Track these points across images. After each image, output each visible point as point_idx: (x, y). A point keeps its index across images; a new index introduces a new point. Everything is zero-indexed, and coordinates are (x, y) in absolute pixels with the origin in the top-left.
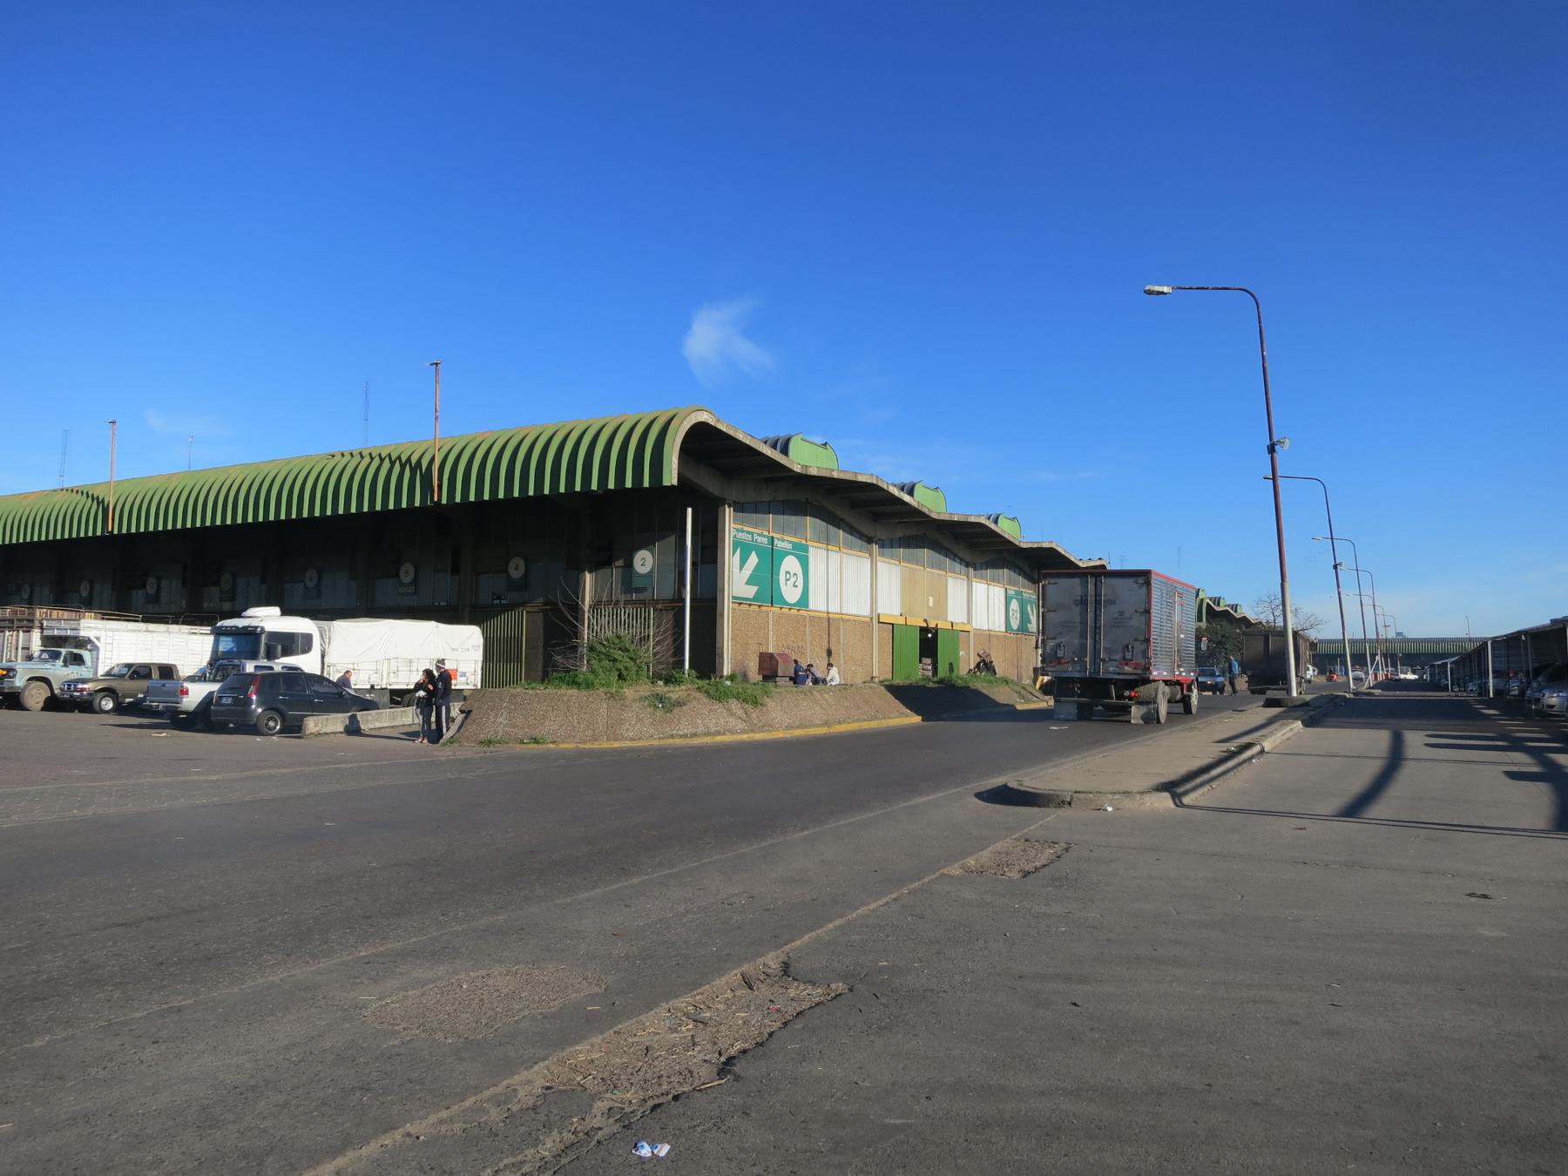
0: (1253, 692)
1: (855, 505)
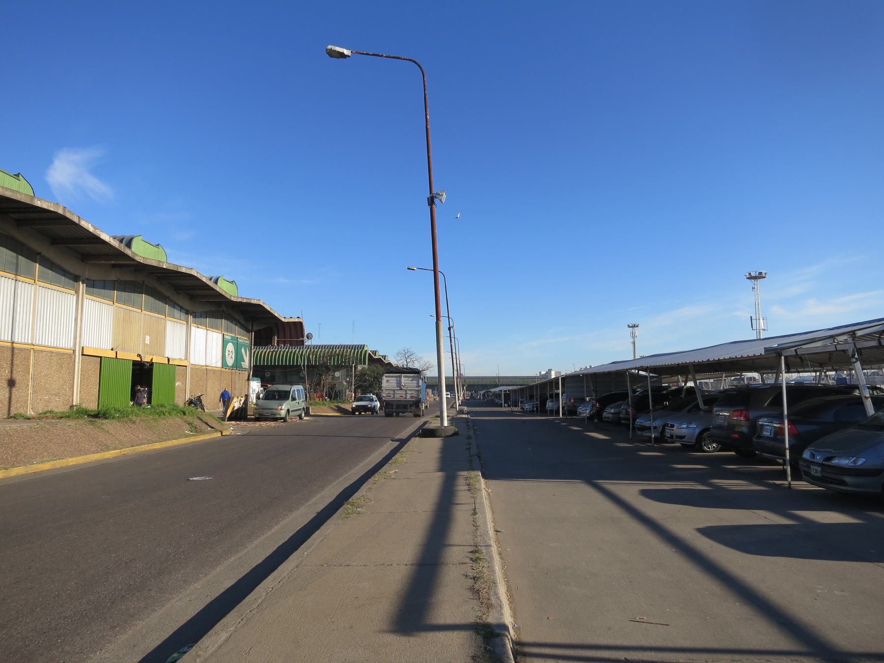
1: (178, 289)
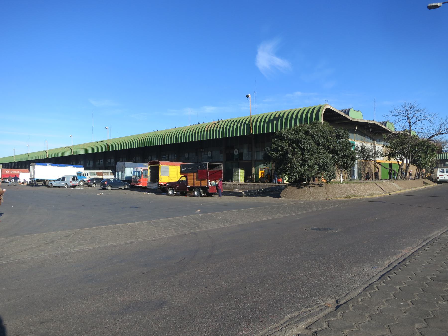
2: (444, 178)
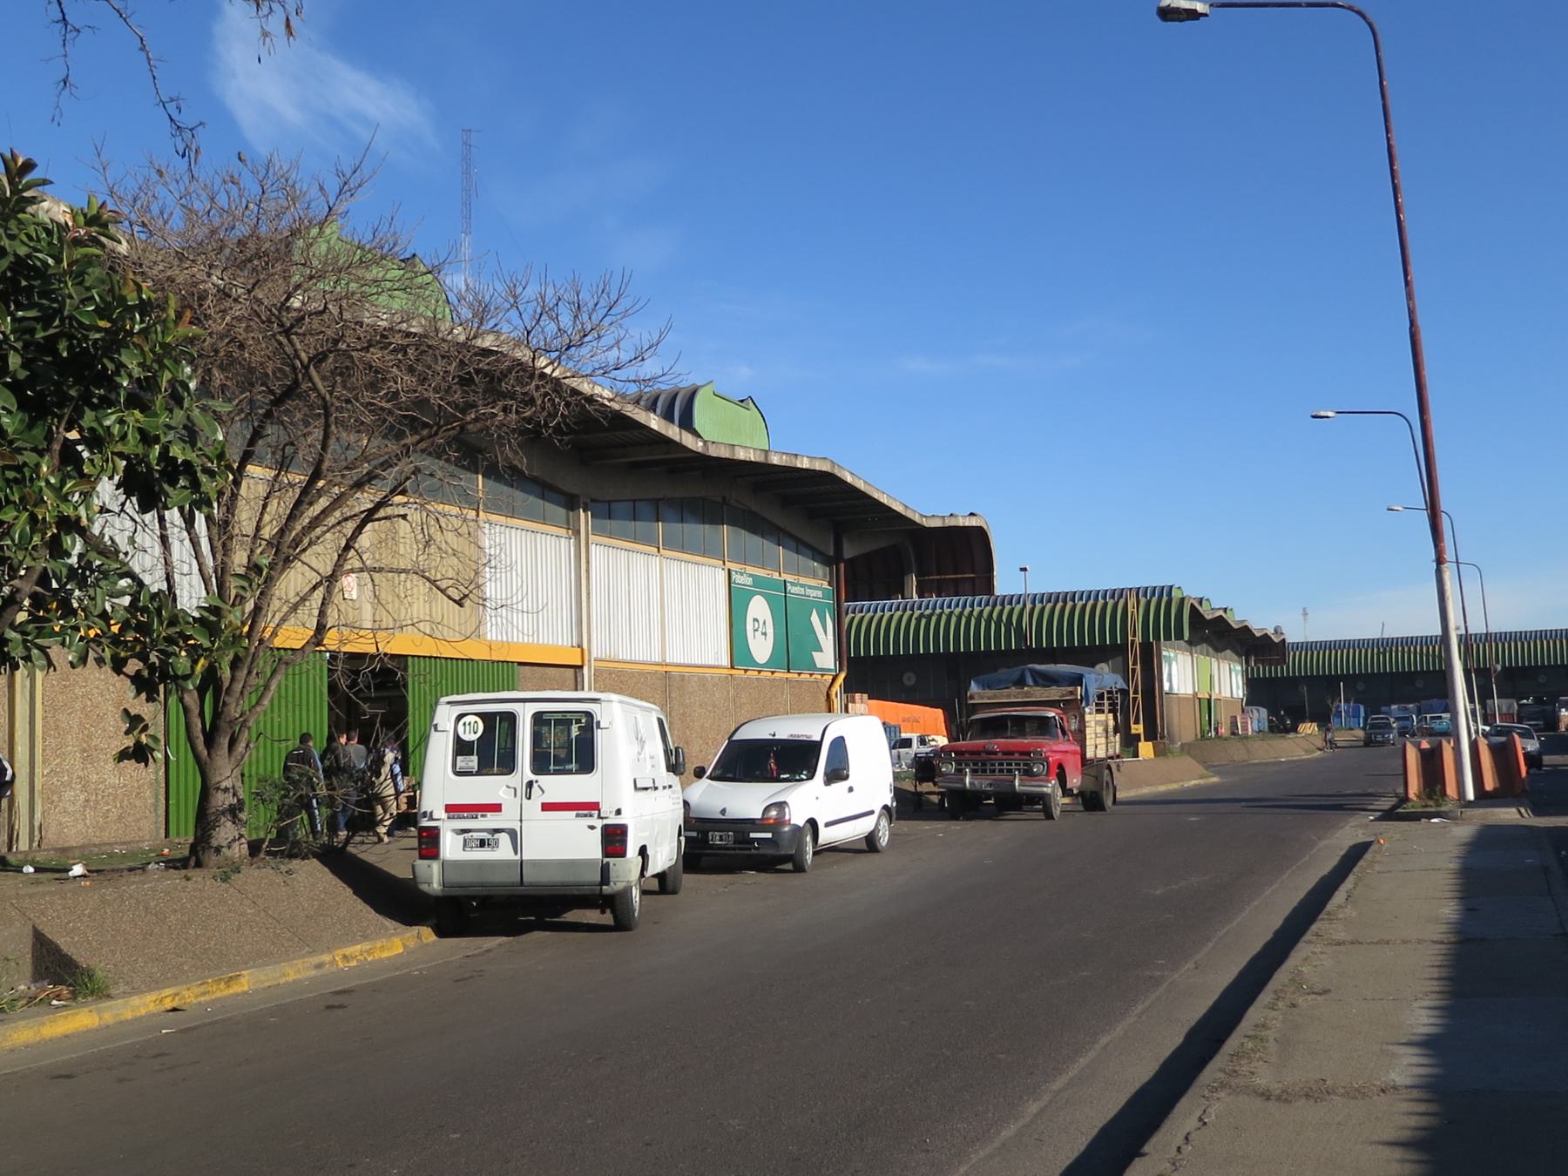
0: (449, 818)
2: (504, 839)
